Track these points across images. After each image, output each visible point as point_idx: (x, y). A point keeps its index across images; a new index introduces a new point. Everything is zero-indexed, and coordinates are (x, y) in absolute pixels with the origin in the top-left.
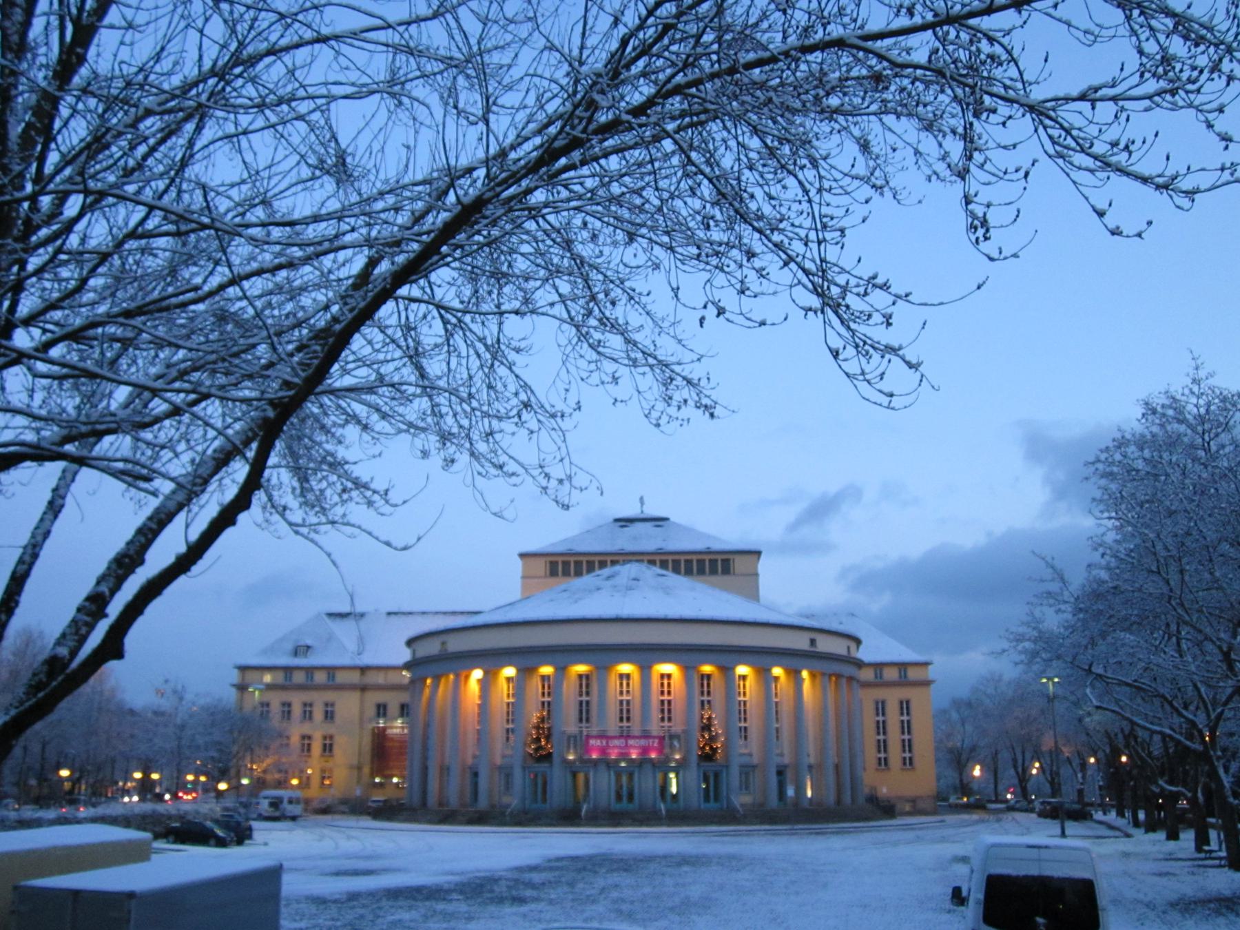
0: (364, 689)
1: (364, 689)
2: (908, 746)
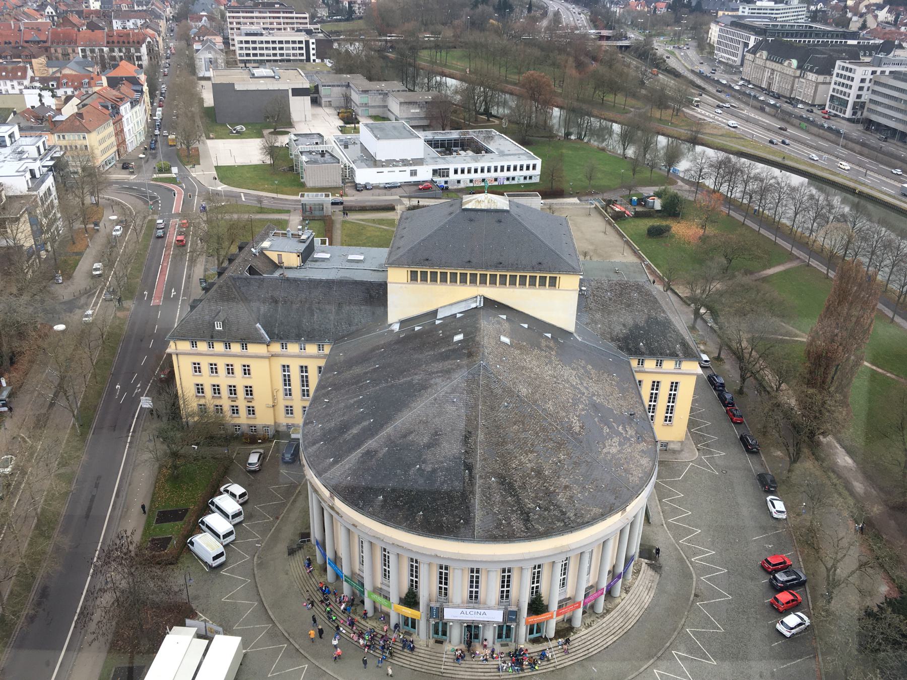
2: (670, 410)
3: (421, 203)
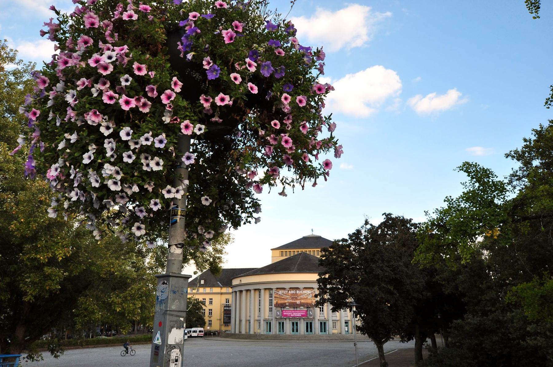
0: (222, 294)
1: (222, 294)
3: (243, 282)
